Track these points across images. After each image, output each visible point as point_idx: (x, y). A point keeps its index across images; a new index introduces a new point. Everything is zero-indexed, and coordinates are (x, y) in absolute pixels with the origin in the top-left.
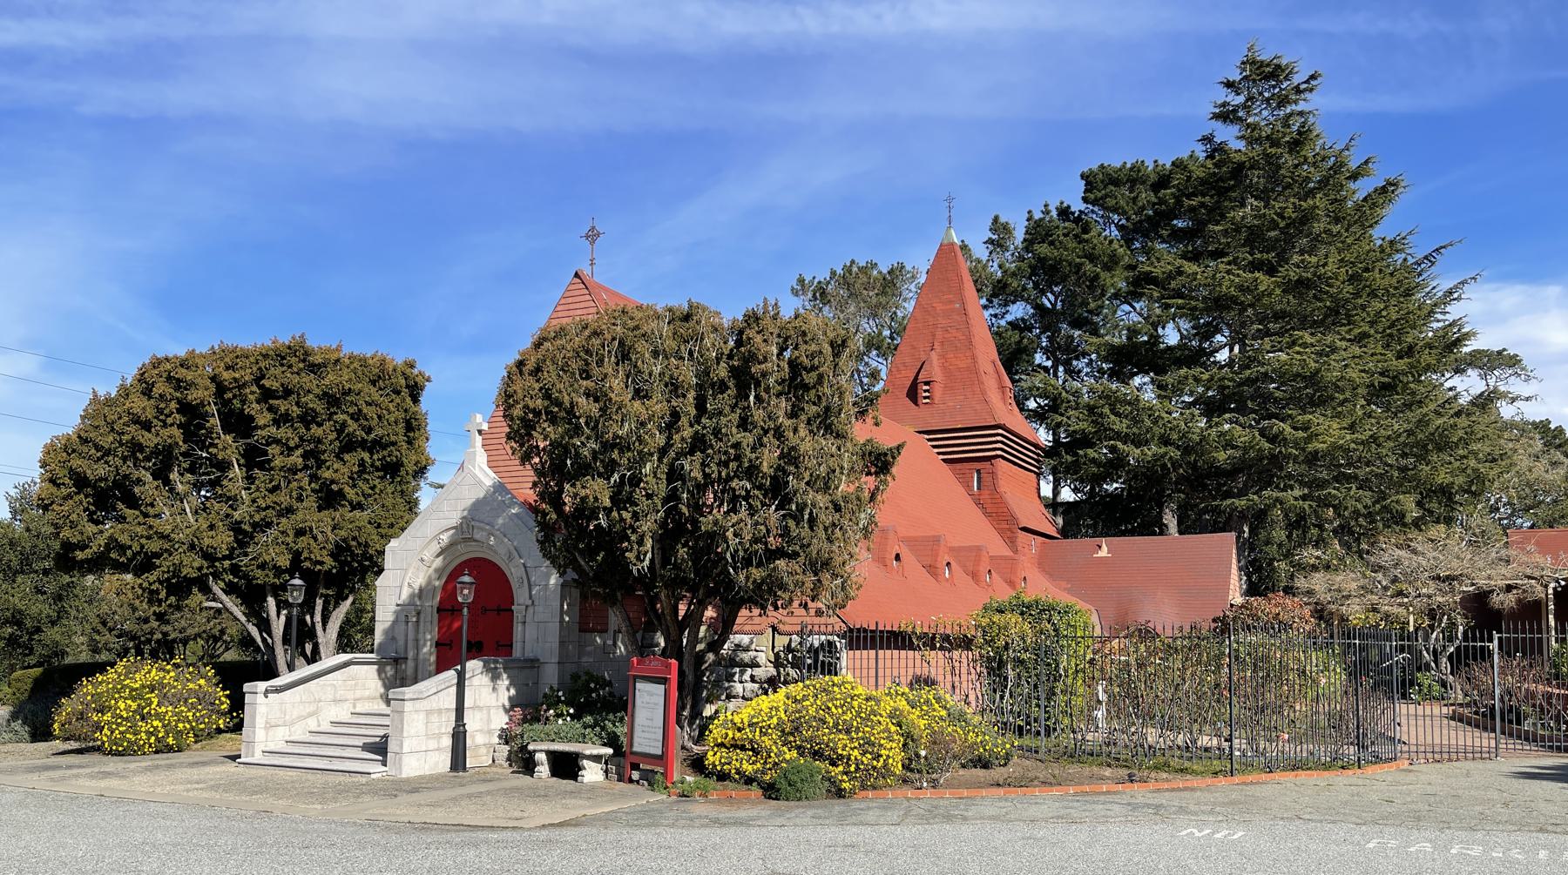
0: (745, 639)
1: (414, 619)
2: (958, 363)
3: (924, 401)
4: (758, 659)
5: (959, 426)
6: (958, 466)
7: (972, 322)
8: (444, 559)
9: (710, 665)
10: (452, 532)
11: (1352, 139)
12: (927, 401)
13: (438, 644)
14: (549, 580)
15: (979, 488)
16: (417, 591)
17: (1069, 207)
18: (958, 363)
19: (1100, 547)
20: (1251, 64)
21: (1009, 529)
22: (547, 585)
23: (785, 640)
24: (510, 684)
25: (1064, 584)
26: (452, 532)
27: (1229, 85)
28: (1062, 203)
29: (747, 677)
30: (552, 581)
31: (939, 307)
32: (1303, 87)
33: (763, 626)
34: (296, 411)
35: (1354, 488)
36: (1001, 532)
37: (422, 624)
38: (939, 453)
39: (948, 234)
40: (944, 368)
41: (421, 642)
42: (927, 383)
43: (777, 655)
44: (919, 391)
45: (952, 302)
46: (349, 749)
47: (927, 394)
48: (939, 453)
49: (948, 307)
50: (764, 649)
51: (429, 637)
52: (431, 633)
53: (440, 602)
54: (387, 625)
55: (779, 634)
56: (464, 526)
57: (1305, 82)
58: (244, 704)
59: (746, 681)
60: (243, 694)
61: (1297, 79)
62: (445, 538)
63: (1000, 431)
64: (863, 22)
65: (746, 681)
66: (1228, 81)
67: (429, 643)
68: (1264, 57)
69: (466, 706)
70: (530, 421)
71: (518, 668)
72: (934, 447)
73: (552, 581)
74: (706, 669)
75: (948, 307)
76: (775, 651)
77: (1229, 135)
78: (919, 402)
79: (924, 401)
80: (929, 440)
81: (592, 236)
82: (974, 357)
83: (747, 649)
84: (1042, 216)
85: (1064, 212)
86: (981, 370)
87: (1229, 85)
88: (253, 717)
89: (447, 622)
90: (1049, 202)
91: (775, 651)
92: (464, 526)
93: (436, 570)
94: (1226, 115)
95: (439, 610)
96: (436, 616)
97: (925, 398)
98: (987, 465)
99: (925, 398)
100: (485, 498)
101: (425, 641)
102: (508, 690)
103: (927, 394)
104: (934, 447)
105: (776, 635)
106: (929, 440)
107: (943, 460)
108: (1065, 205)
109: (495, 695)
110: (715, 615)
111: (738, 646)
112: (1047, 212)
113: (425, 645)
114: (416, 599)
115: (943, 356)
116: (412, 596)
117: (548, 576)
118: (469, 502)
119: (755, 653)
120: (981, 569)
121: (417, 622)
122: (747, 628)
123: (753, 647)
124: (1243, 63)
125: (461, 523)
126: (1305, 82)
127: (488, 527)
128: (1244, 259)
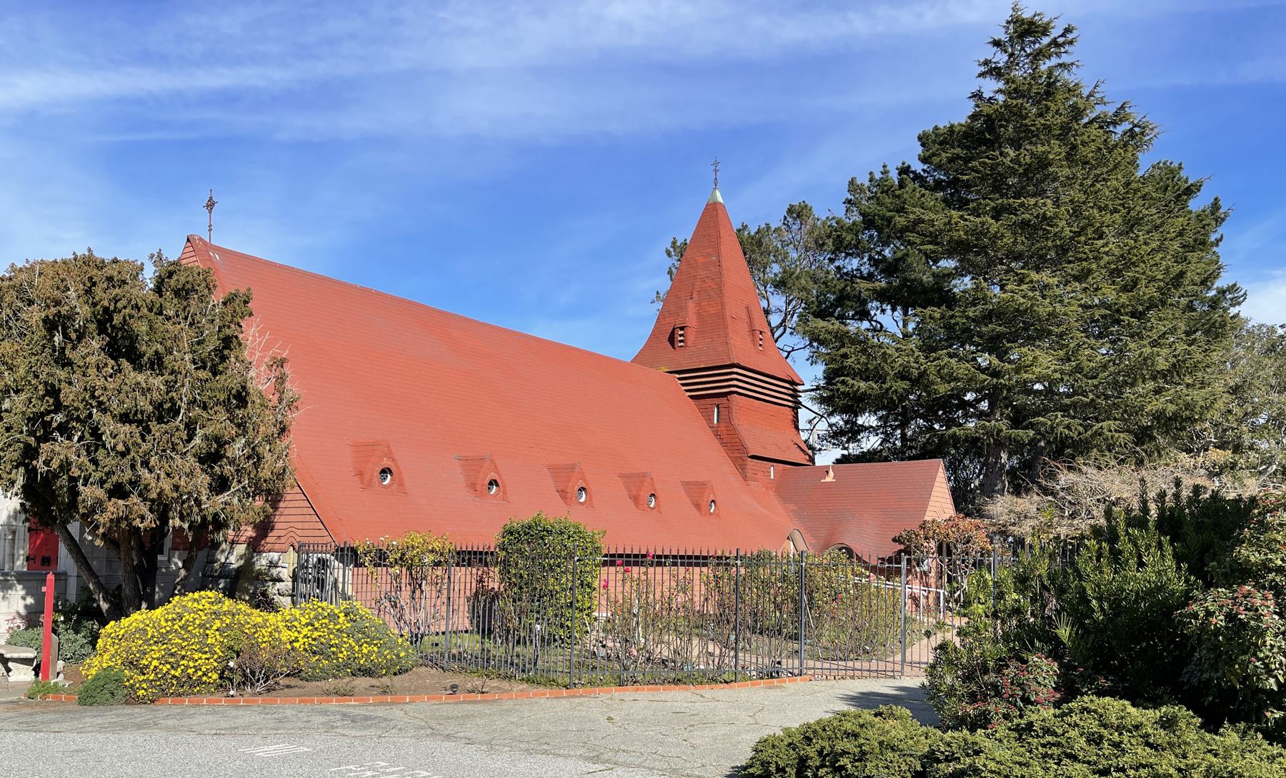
0: (275, 556)
1: (10, 537)
2: (710, 309)
3: (680, 344)
4: (281, 575)
5: (703, 366)
6: (702, 401)
7: (725, 272)
9: (181, 580)
11: (1096, 86)
12: (682, 344)
13: (28, 559)
15: (718, 422)
16: (12, 513)
17: (909, 167)
18: (710, 309)
19: (827, 472)
20: (1015, 23)
21: (740, 458)
24: (27, 594)
25: (792, 507)
27: (997, 43)
28: (903, 164)
31: (700, 260)
32: (1061, 40)
35: (1059, 416)
36: (734, 460)
38: (687, 391)
39: (713, 194)
40: (698, 314)
41: (16, 556)
42: (682, 329)
44: (676, 336)
45: (710, 255)
47: (682, 338)
48: (687, 391)
49: (707, 260)
51: (22, 552)
52: (23, 549)
57: (1061, 36)
61: (1055, 33)
63: (735, 370)
64: (906, 20)
66: (995, 40)
67: (22, 558)
68: (1027, 15)
71: (37, 580)
72: (683, 385)
74: (178, 583)
75: (707, 260)
77: (990, 87)
78: (676, 346)
79: (680, 344)
80: (680, 379)
81: (211, 205)
82: (722, 305)
84: (881, 176)
85: (904, 170)
86: (728, 314)
87: (997, 43)
90: (887, 164)
94: (993, 71)
96: (28, 534)
97: (681, 341)
98: (723, 400)
99: (681, 341)
101: (19, 555)
102: (24, 598)
103: (682, 338)
104: (683, 385)
106: (680, 379)
107: (691, 397)
108: (906, 165)
109: (5, 603)
110: (254, 535)
112: (885, 172)
113: (18, 559)
114: (12, 520)
115: (699, 304)
120: (642, 493)
121: (13, 540)
122: (277, 547)
124: (1008, 22)
126: (1061, 36)
128: (987, 205)
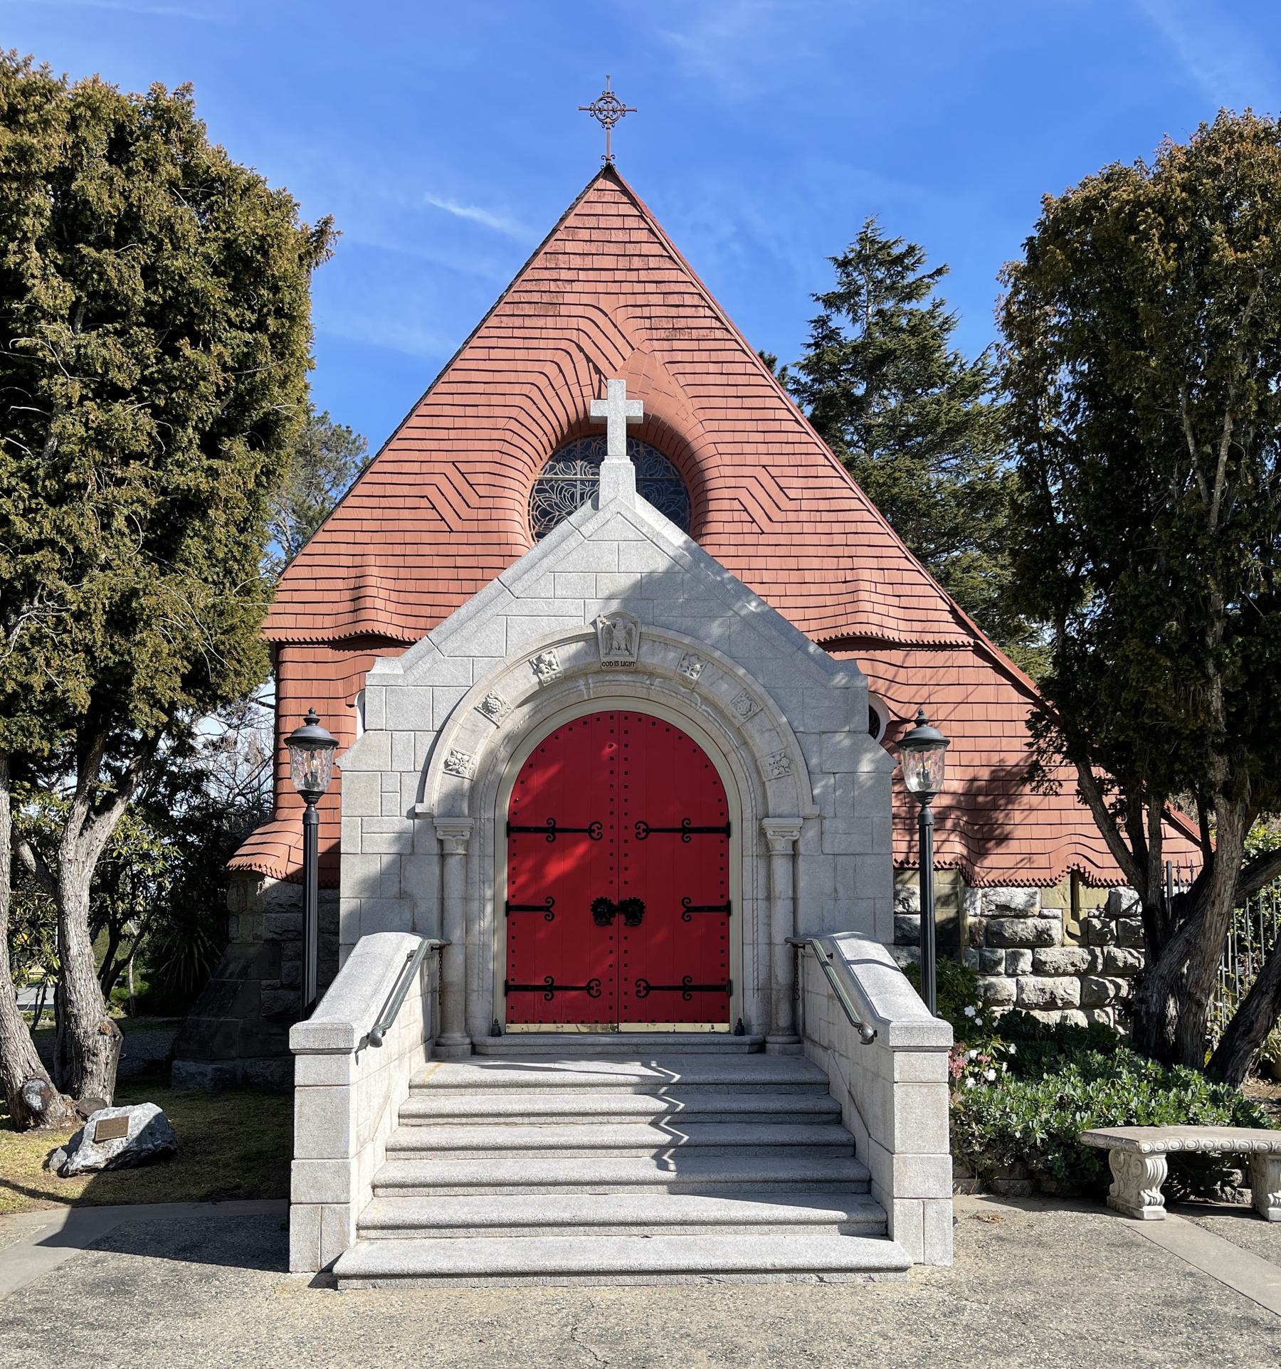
8: (535, 711)
10: (573, 648)
14: (857, 762)
22: (853, 772)
23: (1102, 896)
26: (573, 648)
29: (1025, 963)
30: (865, 766)
33: (1056, 872)
34: (137, 292)
37: (475, 861)
43: (1086, 925)
46: (622, 1194)
50: (1058, 913)
53: (513, 813)
54: (375, 867)
55: (1088, 884)
56: (619, 634)
57: (930, 276)
58: (293, 1087)
59: (1024, 973)
60: (288, 1058)
62: (559, 658)
65: (1024, 973)
69: (298, 1079)
70: (1150, 430)
73: (865, 766)
76: (1082, 915)
83: (1022, 914)
88: (337, 1122)
89: (529, 864)
91: (1082, 915)
92: (619, 634)
93: (509, 738)
95: (510, 829)
100: (669, 572)
101: (483, 900)
105: (1082, 888)
111: (1004, 909)
116: (452, 798)
117: (854, 754)
118: (625, 582)
119: (1041, 923)
123: (1036, 910)
125: (609, 630)
126: (930, 276)
127: (687, 640)
